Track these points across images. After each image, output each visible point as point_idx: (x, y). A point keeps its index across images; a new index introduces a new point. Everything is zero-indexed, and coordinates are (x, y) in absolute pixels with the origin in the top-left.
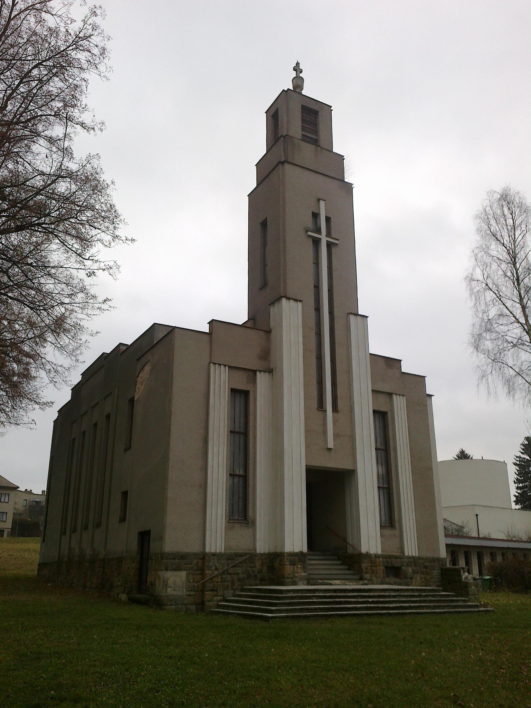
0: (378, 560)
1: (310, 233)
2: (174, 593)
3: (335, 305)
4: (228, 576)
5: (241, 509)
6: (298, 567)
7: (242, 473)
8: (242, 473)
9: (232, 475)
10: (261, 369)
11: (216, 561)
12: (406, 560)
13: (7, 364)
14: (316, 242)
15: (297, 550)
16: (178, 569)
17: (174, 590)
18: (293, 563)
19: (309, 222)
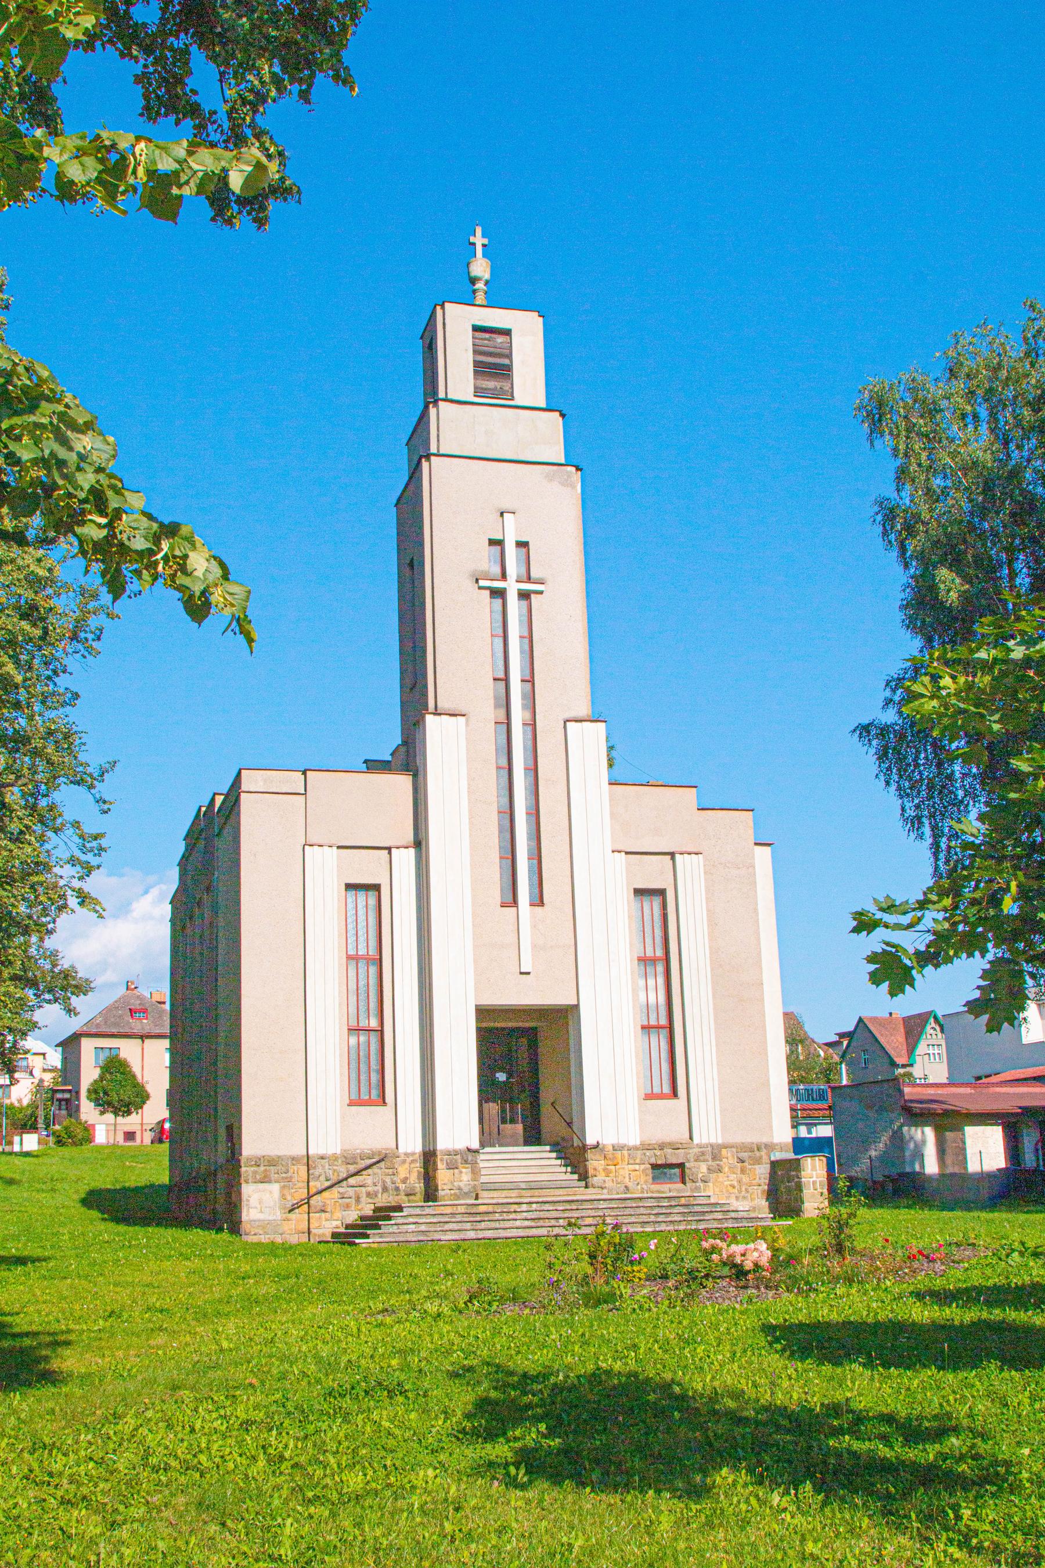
0: (619, 1154)
1: (482, 583)
2: (261, 1216)
3: (419, 379)
4: (349, 1189)
5: (371, 1087)
6: (461, 1172)
7: (374, 1023)
8: (374, 1023)
9: (355, 1030)
10: (399, 844)
11: (327, 1167)
12: (696, 1150)
13: (954, 1305)
14: (499, 594)
15: (461, 1145)
16: (265, 1180)
17: (261, 1212)
18: (451, 1167)
19: (485, 560)
